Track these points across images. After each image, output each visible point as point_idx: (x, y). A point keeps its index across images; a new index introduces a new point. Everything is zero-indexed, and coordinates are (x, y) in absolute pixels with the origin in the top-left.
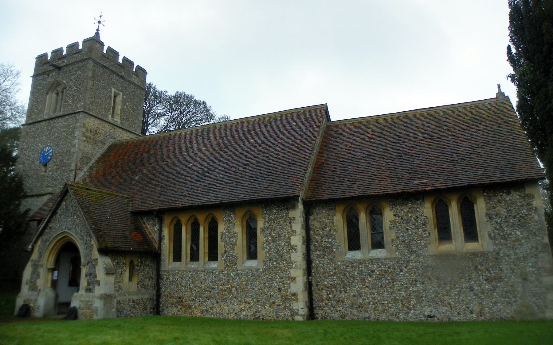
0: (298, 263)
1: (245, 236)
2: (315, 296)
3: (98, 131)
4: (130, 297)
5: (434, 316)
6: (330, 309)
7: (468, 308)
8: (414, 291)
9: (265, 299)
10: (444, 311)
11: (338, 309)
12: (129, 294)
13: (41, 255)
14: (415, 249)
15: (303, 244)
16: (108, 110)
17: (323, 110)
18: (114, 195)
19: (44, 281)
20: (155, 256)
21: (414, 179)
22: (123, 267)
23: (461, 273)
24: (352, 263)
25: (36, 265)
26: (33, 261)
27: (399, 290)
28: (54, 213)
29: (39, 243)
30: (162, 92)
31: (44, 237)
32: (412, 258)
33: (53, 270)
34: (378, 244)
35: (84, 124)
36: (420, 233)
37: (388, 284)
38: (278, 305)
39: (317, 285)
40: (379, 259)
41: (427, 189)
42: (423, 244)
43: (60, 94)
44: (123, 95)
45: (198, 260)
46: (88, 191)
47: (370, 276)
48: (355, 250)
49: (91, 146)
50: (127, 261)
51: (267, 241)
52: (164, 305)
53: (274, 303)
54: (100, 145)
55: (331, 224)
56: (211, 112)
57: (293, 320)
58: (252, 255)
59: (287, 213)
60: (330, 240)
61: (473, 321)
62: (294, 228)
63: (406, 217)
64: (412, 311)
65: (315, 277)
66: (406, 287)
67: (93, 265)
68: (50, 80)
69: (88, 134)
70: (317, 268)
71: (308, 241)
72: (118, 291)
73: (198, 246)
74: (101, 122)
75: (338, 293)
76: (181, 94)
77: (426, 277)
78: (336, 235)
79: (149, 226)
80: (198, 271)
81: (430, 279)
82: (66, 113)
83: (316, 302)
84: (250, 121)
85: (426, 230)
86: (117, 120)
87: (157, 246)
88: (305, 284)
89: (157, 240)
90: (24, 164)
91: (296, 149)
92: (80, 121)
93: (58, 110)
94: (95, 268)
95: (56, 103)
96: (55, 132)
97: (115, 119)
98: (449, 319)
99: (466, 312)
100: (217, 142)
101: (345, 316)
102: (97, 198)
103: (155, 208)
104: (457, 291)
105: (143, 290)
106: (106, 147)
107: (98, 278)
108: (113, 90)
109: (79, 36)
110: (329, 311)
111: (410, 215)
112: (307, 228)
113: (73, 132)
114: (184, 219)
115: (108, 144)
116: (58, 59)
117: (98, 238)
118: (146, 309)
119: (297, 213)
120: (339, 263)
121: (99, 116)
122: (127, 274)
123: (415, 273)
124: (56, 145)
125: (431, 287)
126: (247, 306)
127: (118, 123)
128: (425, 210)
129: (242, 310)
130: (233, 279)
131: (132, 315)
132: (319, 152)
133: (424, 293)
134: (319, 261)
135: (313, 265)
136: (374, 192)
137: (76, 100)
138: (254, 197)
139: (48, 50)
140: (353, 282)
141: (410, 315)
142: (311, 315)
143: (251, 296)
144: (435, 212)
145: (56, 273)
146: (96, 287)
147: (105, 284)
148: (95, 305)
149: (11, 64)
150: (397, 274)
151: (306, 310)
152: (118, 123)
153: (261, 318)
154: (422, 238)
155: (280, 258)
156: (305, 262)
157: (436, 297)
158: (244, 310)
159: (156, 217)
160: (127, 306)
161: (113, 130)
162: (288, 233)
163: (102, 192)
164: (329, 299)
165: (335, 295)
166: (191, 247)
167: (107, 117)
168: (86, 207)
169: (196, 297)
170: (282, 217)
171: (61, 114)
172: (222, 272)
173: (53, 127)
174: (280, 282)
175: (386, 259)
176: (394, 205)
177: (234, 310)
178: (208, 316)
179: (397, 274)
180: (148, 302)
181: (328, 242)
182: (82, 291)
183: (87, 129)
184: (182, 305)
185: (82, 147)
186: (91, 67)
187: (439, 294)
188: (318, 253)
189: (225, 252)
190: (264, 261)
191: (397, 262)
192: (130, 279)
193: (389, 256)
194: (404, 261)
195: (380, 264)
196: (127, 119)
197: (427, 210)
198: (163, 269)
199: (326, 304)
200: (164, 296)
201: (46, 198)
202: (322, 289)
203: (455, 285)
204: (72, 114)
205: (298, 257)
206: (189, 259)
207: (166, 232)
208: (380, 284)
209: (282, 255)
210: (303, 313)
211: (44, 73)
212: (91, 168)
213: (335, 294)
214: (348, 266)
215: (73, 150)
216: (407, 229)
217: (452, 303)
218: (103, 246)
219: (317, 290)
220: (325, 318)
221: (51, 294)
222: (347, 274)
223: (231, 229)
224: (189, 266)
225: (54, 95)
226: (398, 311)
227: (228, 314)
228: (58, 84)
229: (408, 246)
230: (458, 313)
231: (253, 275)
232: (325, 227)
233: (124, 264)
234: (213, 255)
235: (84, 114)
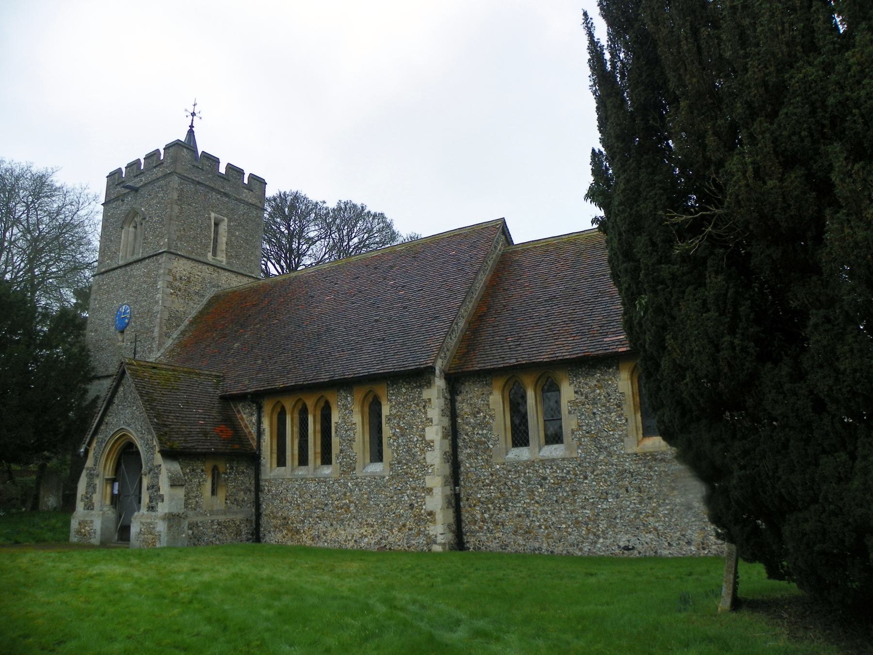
0: (436, 467)
1: (367, 427)
2: (465, 516)
3: (192, 278)
4: (213, 518)
5: (633, 548)
6: (485, 535)
7: (684, 535)
8: (604, 509)
9: (393, 519)
10: (648, 540)
11: (497, 535)
12: (212, 513)
14: (606, 444)
15: (445, 437)
17: (501, 228)
18: (196, 374)
19: (101, 496)
20: (254, 459)
21: (606, 336)
22: (202, 476)
23: (673, 481)
24: (515, 467)
25: (91, 475)
26: (87, 469)
27: (583, 507)
29: (94, 444)
30: (317, 203)
31: (100, 436)
32: (601, 457)
33: (113, 481)
34: (554, 438)
35: (170, 270)
36: (613, 419)
37: (566, 498)
38: (410, 529)
39: (467, 500)
40: (553, 460)
41: (620, 350)
42: (617, 436)
44: (229, 221)
45: (307, 464)
46: (154, 371)
48: (521, 446)
49: (182, 301)
50: (209, 466)
51: (394, 435)
52: (265, 530)
53: (404, 525)
54: (196, 298)
55: (486, 408)
56: (394, 228)
57: (430, 550)
58: (377, 456)
60: (485, 432)
61: (691, 557)
63: (592, 395)
64: (601, 540)
65: (464, 487)
66: (593, 503)
67: (155, 473)
70: (467, 474)
71: (453, 433)
72: (195, 509)
74: (196, 264)
75: (496, 512)
76: (346, 204)
77: (621, 487)
78: (494, 424)
79: (244, 416)
80: (307, 479)
81: (627, 491)
82: (146, 255)
83: (466, 525)
84: (395, 251)
85: (622, 414)
86: (222, 258)
87: (254, 444)
89: (255, 436)
91: (446, 294)
94: (157, 477)
96: (134, 283)
97: (218, 258)
98: (656, 552)
99: (681, 542)
100: (346, 286)
101: (507, 545)
102: (168, 380)
103: (249, 390)
104: (667, 510)
105: (235, 508)
106: (205, 301)
107: (161, 492)
108: (213, 215)
110: (484, 538)
111: (598, 391)
112: (452, 413)
113: (155, 283)
114: (288, 404)
115: (209, 296)
116: (135, 177)
118: (240, 535)
119: (435, 393)
120: (498, 467)
121: (193, 256)
122: (208, 485)
123: (606, 481)
124: (136, 302)
125: (628, 503)
126: (370, 530)
128: (620, 383)
129: (363, 536)
130: (351, 491)
131: (218, 542)
132: (483, 296)
133: (619, 512)
134: (470, 464)
135: (462, 469)
136: (544, 358)
137: (158, 236)
138: (373, 371)
140: (517, 495)
141: (599, 546)
142: (459, 543)
143: (375, 515)
144: (636, 386)
145: (116, 485)
146: (160, 504)
147: (171, 499)
148: (158, 529)
149: (84, 186)
150: (579, 483)
151: (450, 536)
152: (224, 263)
153: (388, 547)
157: (635, 518)
158: (366, 536)
159: (253, 402)
160: (210, 530)
162: (422, 422)
163: (176, 371)
164: (484, 521)
165: (492, 515)
167: (205, 256)
168: (147, 393)
169: (305, 517)
170: (414, 399)
171: (140, 256)
173: (130, 277)
174: (412, 495)
175: (563, 459)
176: (575, 376)
177: (353, 536)
178: (320, 544)
180: (243, 525)
181: (482, 434)
182: (144, 510)
183: (174, 277)
184: (288, 530)
185: (168, 304)
186: (176, 186)
187: (641, 513)
188: (468, 451)
189: (341, 451)
190: (391, 465)
191: (580, 465)
192: (214, 492)
194: (589, 463)
195: (555, 467)
196: (237, 257)
198: (263, 477)
199: (481, 528)
200: (266, 515)
202: (475, 506)
203: (664, 500)
204: (153, 256)
205: (435, 458)
206: (296, 462)
207: (266, 424)
208: (555, 499)
210: (443, 541)
211: (116, 199)
212: (183, 333)
213: (492, 512)
214: (510, 471)
216: (594, 414)
217: (660, 528)
218: (167, 447)
219: (467, 506)
220: (479, 548)
221: (111, 513)
222: (509, 483)
223: (348, 416)
224: (296, 473)
225: (131, 229)
226: (580, 539)
227: (345, 541)
228: (136, 214)
229: (595, 439)
230: (669, 543)
231: (377, 485)
232: (478, 413)
233: (202, 471)
234: (326, 459)
235: (169, 256)
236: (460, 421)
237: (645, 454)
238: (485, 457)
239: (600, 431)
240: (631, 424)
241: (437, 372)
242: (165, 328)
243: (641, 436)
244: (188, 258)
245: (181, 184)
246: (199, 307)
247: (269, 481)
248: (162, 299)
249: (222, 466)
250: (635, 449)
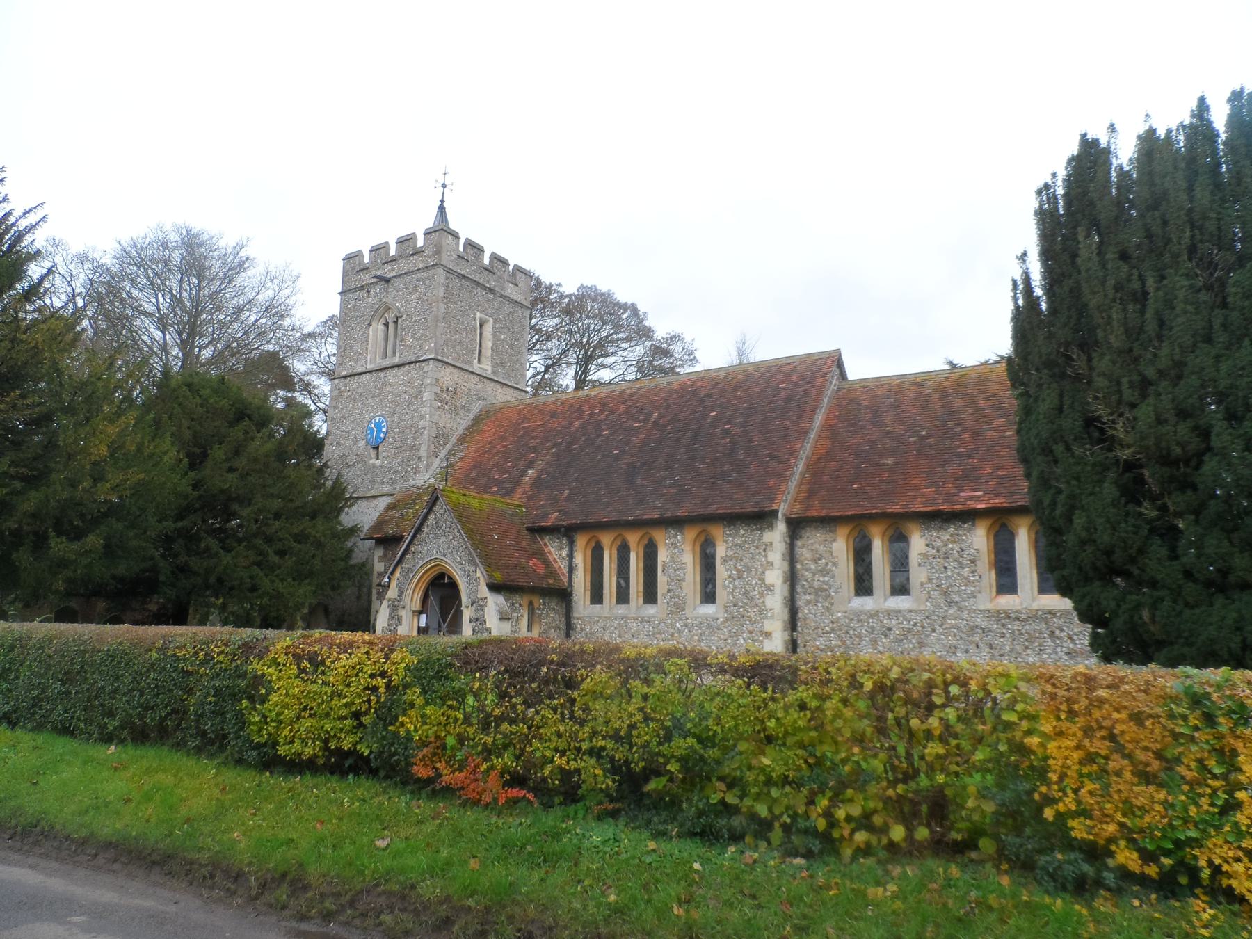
0: (776, 611)
13: (401, 593)
15: (785, 582)
16: (472, 351)
17: (835, 361)
20: (564, 595)
24: (858, 616)
28: (419, 530)
29: (398, 574)
32: (951, 612)
34: (901, 589)
35: (437, 380)
40: (900, 611)
43: (391, 325)
47: (886, 636)
54: (462, 412)
58: (709, 596)
59: (761, 536)
62: (770, 559)
69: (444, 395)
70: (805, 620)
71: (792, 578)
73: (627, 580)
77: (971, 643)
80: (628, 618)
86: (487, 367)
88: (786, 642)
89: (566, 571)
90: (338, 444)
92: (430, 374)
93: (389, 353)
96: (389, 392)
106: (471, 416)
107: (488, 625)
108: (478, 315)
113: (420, 393)
114: (607, 539)
115: (476, 408)
117: (487, 565)
119: (777, 535)
127: (489, 374)
130: (679, 632)
135: (800, 615)
137: (420, 339)
144: (992, 543)
145: (423, 617)
154: (968, 582)
155: (749, 603)
156: (786, 610)
161: (481, 386)
166: (618, 583)
167: (470, 363)
170: (753, 542)
171: (396, 360)
172: (663, 621)
173: (384, 384)
179: (927, 636)
188: (808, 597)
189: (669, 591)
193: (915, 607)
196: (502, 365)
197: (979, 538)
198: (575, 615)
205: (776, 603)
206: (614, 600)
207: (579, 559)
209: (751, 599)
215: (421, 424)
225: (381, 327)
229: (945, 593)
231: (709, 626)
234: (650, 596)
235: (436, 363)
236: (799, 566)
237: (998, 612)
238: (826, 604)
239: (951, 585)
240: (985, 581)
241: (780, 515)
242: (432, 447)
243: (994, 593)
244: (454, 366)
245: (447, 278)
246: (465, 423)
247: (582, 619)
248: (429, 416)
249: (538, 601)
250: (990, 606)
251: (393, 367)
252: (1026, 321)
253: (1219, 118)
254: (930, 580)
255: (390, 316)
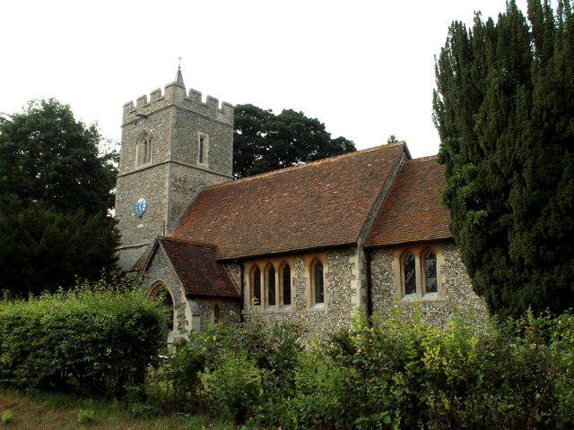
16: (196, 156)
20: (239, 301)
24: (408, 306)
28: (150, 264)
34: (433, 289)
40: (430, 302)
45: (274, 304)
58: (320, 299)
68: (138, 129)
69: (178, 183)
86: (206, 165)
89: (240, 286)
95: (146, 152)
106: (196, 195)
109: (161, 80)
115: (198, 190)
119: (356, 260)
139: (133, 98)
171: (150, 164)
188: (378, 296)
189: (297, 296)
196: (216, 163)
201: (143, 249)
205: (356, 300)
207: (247, 279)
223: (301, 274)
225: (143, 145)
228: (146, 134)
229: (456, 289)
234: (287, 300)
249: (221, 305)
251: (149, 168)
252: (444, 132)
253: (496, 21)
254: (448, 282)
255: (148, 139)
